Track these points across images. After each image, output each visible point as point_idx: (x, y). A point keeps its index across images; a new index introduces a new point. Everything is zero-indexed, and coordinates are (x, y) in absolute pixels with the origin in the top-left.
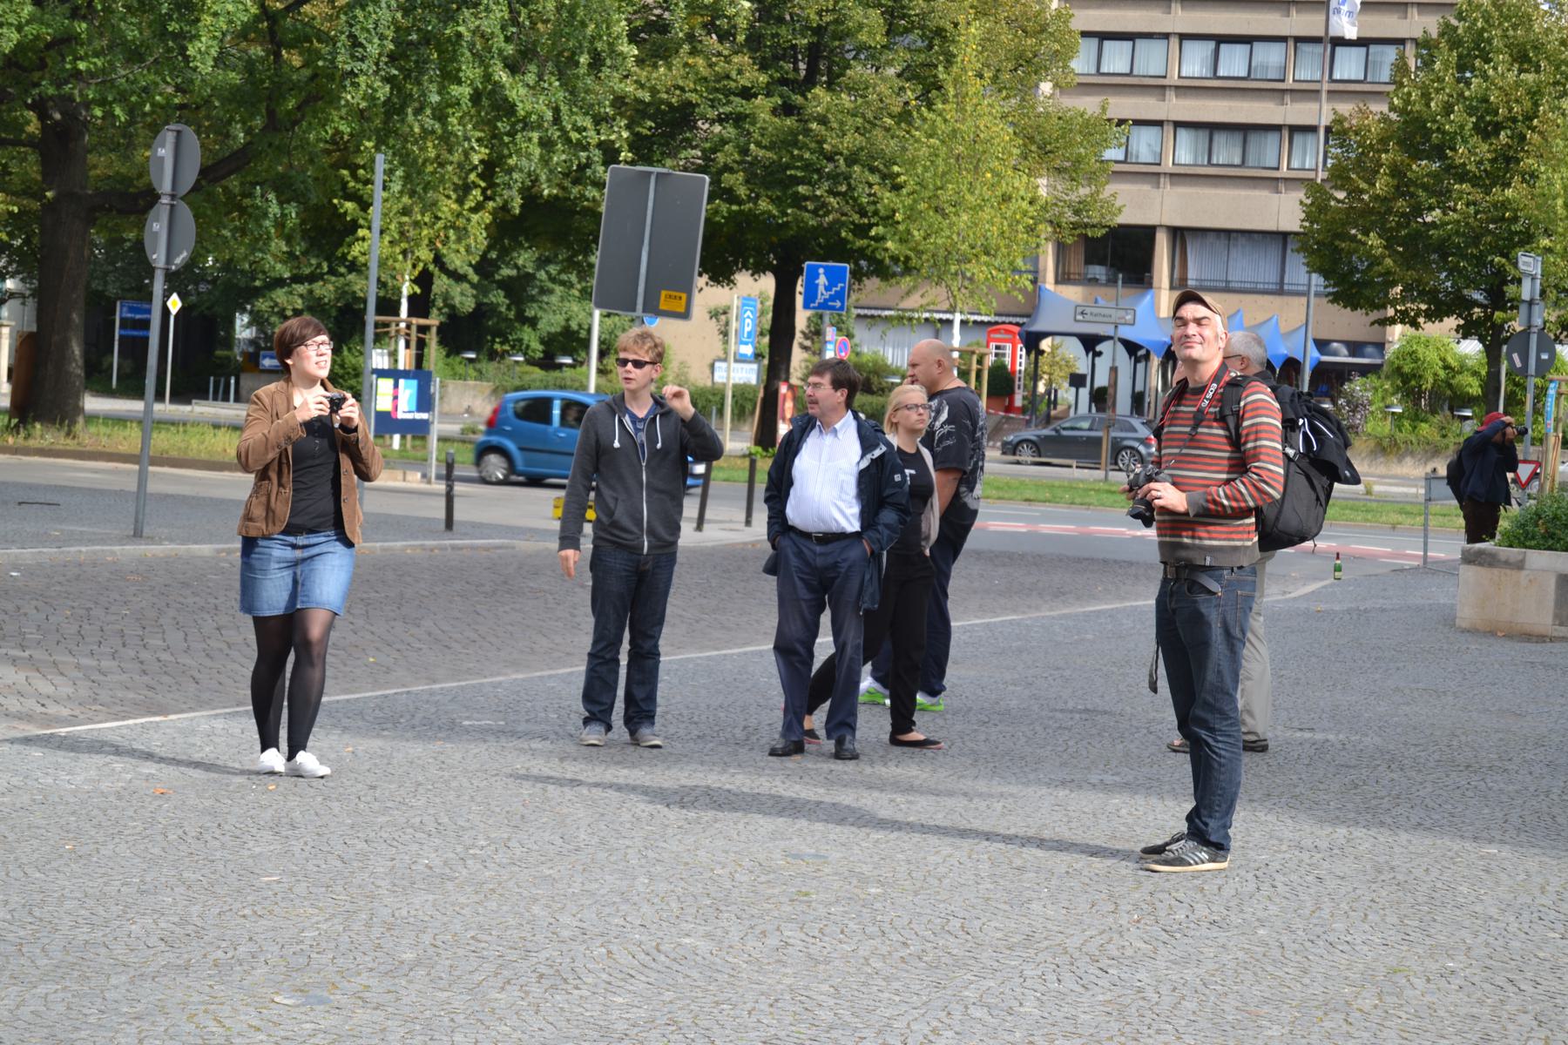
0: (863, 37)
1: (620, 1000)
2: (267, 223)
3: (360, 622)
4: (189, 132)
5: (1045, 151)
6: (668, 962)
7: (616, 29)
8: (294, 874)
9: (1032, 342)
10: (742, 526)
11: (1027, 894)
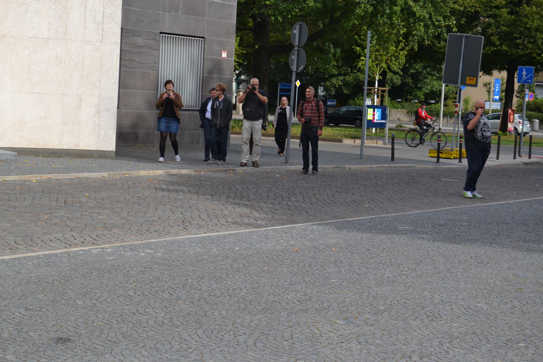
1: (456, 325)
6: (472, 312)
8: (342, 279)
10: (495, 160)
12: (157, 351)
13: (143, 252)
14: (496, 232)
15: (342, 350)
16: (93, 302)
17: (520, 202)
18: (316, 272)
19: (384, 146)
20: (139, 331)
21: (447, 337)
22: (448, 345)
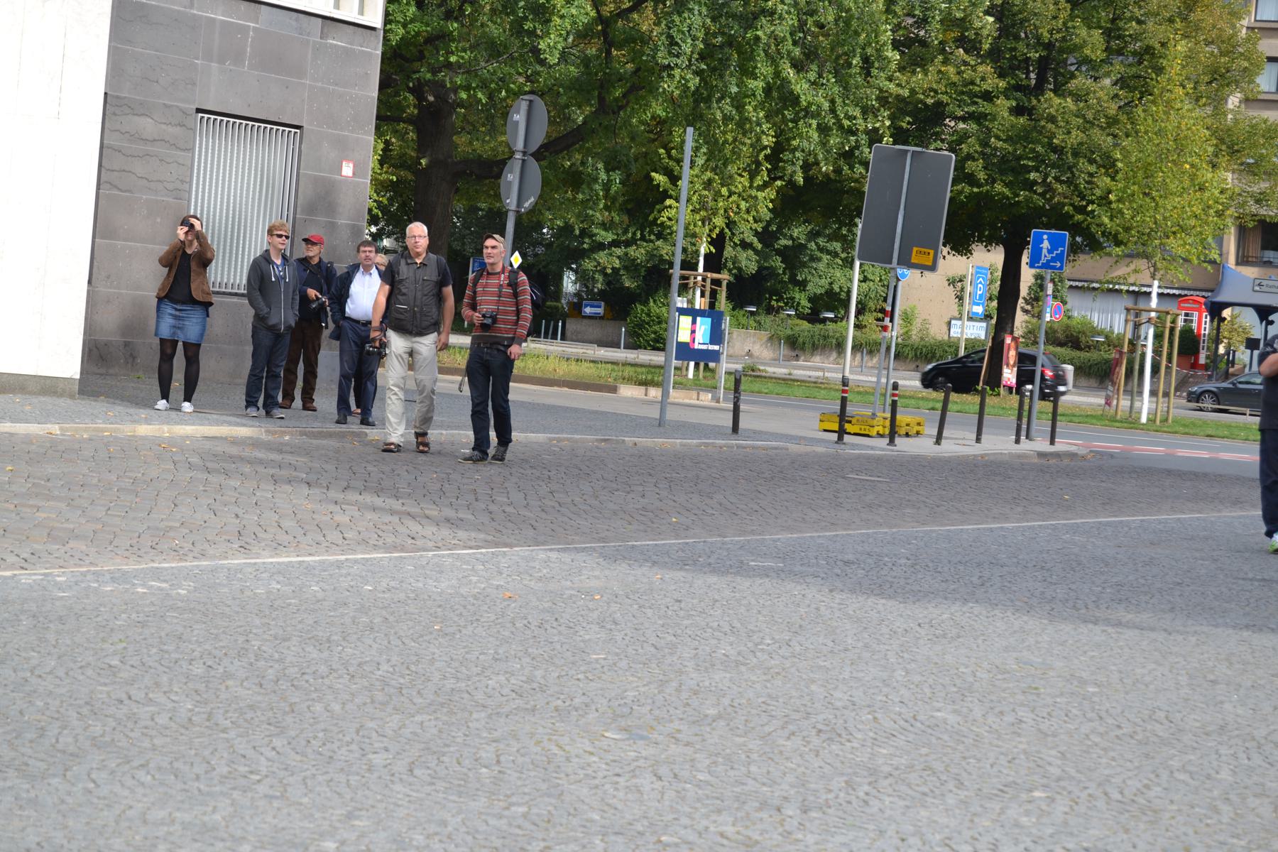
0: (1087, 52)
1: (885, 751)
2: (597, 187)
3: (664, 493)
4: (540, 104)
5: (1233, 152)
6: (923, 728)
7: (883, 38)
8: (617, 654)
9: (1215, 310)
11: (1219, 698)
12: (176, 776)
13: (143, 586)
14: (975, 580)
15: (616, 789)
16: (21, 674)
17: (1030, 528)
18: (556, 639)
19: (714, 404)
20: (132, 735)
21: (865, 773)
22: (866, 788)
